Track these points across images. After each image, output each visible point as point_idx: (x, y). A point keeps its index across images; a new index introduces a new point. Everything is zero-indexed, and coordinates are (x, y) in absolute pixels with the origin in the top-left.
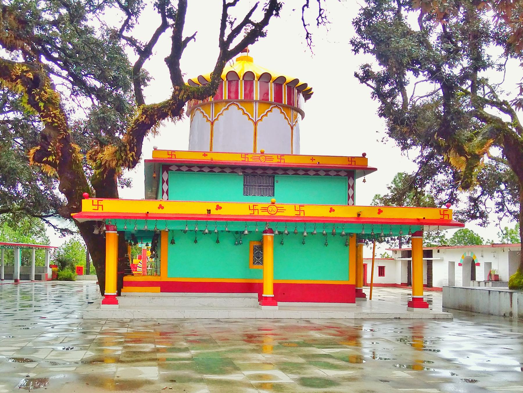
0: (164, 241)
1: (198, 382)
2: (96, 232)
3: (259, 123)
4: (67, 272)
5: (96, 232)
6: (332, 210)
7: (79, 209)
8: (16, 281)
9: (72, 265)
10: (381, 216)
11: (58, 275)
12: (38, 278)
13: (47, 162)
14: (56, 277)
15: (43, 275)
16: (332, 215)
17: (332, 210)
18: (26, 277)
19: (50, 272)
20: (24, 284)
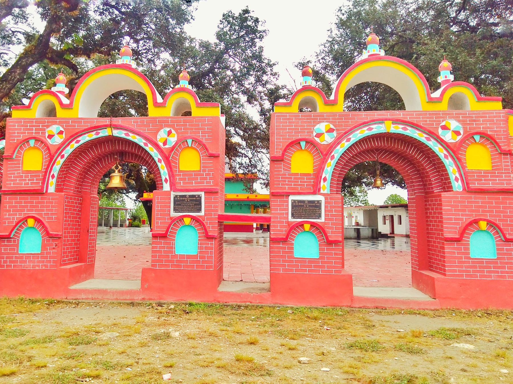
0: (366, 232)
1: (95, 290)
2: (148, 205)
3: (508, 236)
4: (136, 222)
5: (148, 205)
6: (237, 196)
7: (142, 196)
8: (111, 227)
9: (140, 219)
10: (257, 198)
11: (132, 225)
12: (122, 226)
13: (131, 179)
14: (131, 225)
15: (124, 224)
16: (238, 198)
17: (237, 196)
18: (115, 225)
19: (127, 222)
20: (114, 229)
